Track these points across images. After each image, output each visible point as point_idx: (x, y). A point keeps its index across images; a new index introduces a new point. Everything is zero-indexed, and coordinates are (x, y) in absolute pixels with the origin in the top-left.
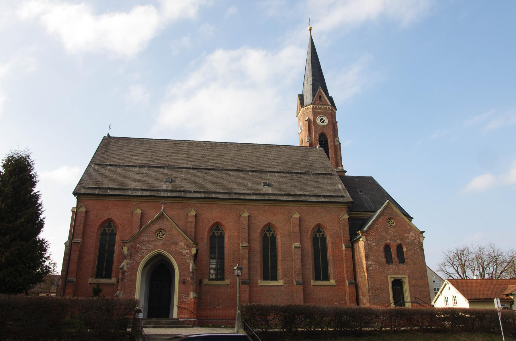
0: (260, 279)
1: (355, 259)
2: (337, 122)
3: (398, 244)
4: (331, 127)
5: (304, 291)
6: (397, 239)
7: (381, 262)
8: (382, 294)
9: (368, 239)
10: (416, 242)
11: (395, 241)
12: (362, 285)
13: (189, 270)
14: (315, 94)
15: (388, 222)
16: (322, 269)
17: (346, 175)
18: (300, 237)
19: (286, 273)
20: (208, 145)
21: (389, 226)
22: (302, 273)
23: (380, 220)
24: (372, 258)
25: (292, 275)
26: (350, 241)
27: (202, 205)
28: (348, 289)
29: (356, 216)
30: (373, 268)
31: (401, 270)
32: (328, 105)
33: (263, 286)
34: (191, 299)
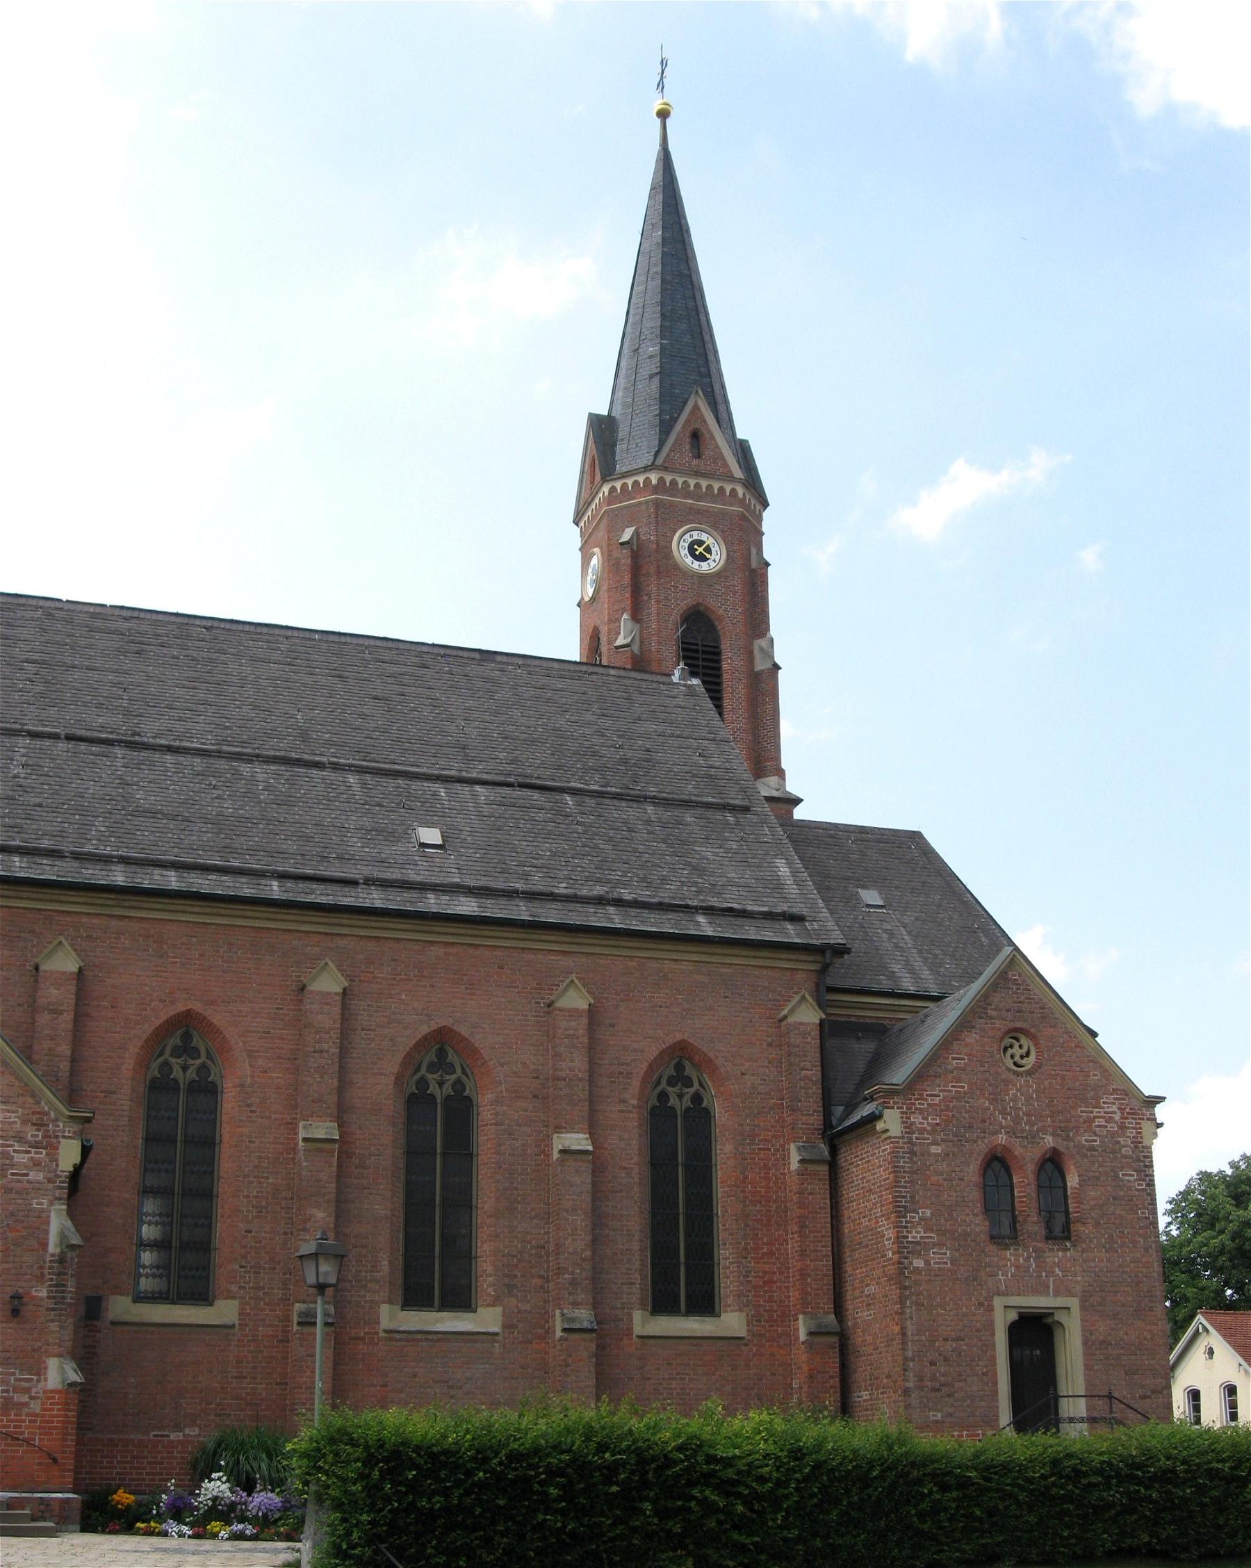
0: (390, 1302)
1: (842, 1215)
2: (768, 564)
3: (1044, 1154)
4: (737, 582)
5: (598, 1365)
6: (1043, 1130)
7: (966, 1235)
8: (965, 1380)
9: (913, 1124)
10: (1124, 1146)
11: (1033, 1138)
12: (869, 1338)
13: (44, 1245)
14: (674, 420)
15: (1005, 1049)
16: (687, 1257)
17: (796, 817)
18: (591, 1102)
19: (516, 1276)
20: (145, 627)
21: (1009, 1070)
22: (594, 1280)
23: (971, 1038)
24: (928, 1213)
25: (542, 1287)
26: (824, 1133)
27: (114, 923)
28: (804, 1357)
29: (849, 1016)
30: (927, 1263)
31: (1051, 1273)
32: (730, 478)
33: (423, 1336)
34: (52, 1391)
